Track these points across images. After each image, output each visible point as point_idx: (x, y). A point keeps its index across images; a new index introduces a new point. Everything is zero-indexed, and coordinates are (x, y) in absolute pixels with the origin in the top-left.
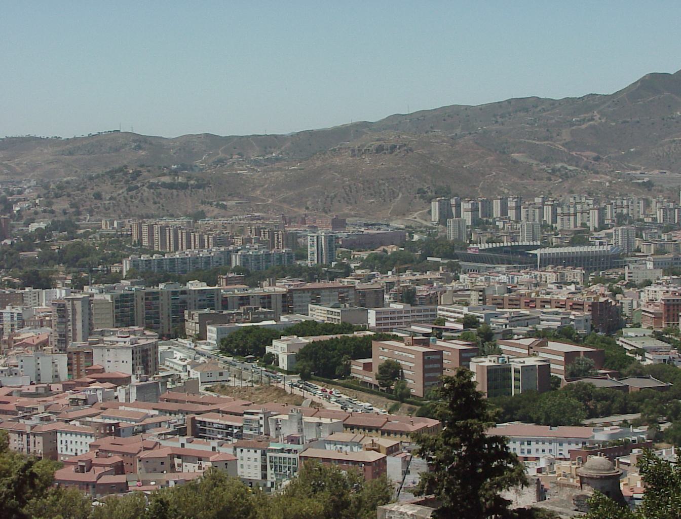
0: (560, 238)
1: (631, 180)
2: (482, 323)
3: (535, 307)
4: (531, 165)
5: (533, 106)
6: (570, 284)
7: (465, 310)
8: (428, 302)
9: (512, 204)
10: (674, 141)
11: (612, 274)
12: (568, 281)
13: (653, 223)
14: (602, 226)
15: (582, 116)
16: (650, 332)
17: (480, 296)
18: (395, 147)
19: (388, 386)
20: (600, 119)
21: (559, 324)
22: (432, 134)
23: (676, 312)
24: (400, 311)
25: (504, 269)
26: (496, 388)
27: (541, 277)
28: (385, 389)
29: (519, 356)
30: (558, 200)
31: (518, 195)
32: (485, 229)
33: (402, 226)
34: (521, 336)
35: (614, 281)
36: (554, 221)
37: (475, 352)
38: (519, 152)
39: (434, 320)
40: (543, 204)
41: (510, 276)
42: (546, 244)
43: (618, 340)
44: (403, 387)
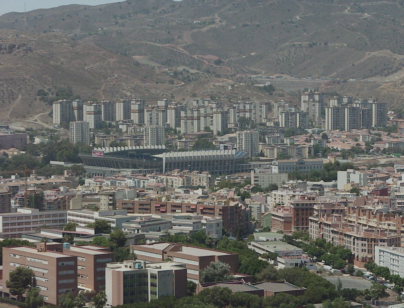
0: (184, 142)
1: (253, 84)
2: (113, 228)
3: (165, 212)
4: (154, 68)
5: (154, 8)
6: (197, 188)
7: (96, 215)
8: (56, 207)
9: (135, 107)
10: (294, 45)
11: (237, 178)
12: (194, 185)
13: (275, 127)
14: (225, 131)
15: (203, 19)
16: (281, 236)
17: (110, 200)
18: (14, 46)
19: (20, 294)
20: (220, 22)
21: (191, 228)
22: (51, 33)
23: (304, 216)
24: (27, 217)
25: (129, 173)
26: (132, 294)
27: (167, 181)
28: (16, 297)
29: (153, 261)
30: (181, 104)
31: (140, 98)
32: (108, 133)
33: (22, 129)
34: (153, 241)
35: (239, 186)
36: (178, 124)
37: (109, 258)
38: (141, 55)
39: (64, 225)
40: (166, 107)
41: (136, 180)
42: (170, 148)
43: (250, 244)
44: (36, 295)
